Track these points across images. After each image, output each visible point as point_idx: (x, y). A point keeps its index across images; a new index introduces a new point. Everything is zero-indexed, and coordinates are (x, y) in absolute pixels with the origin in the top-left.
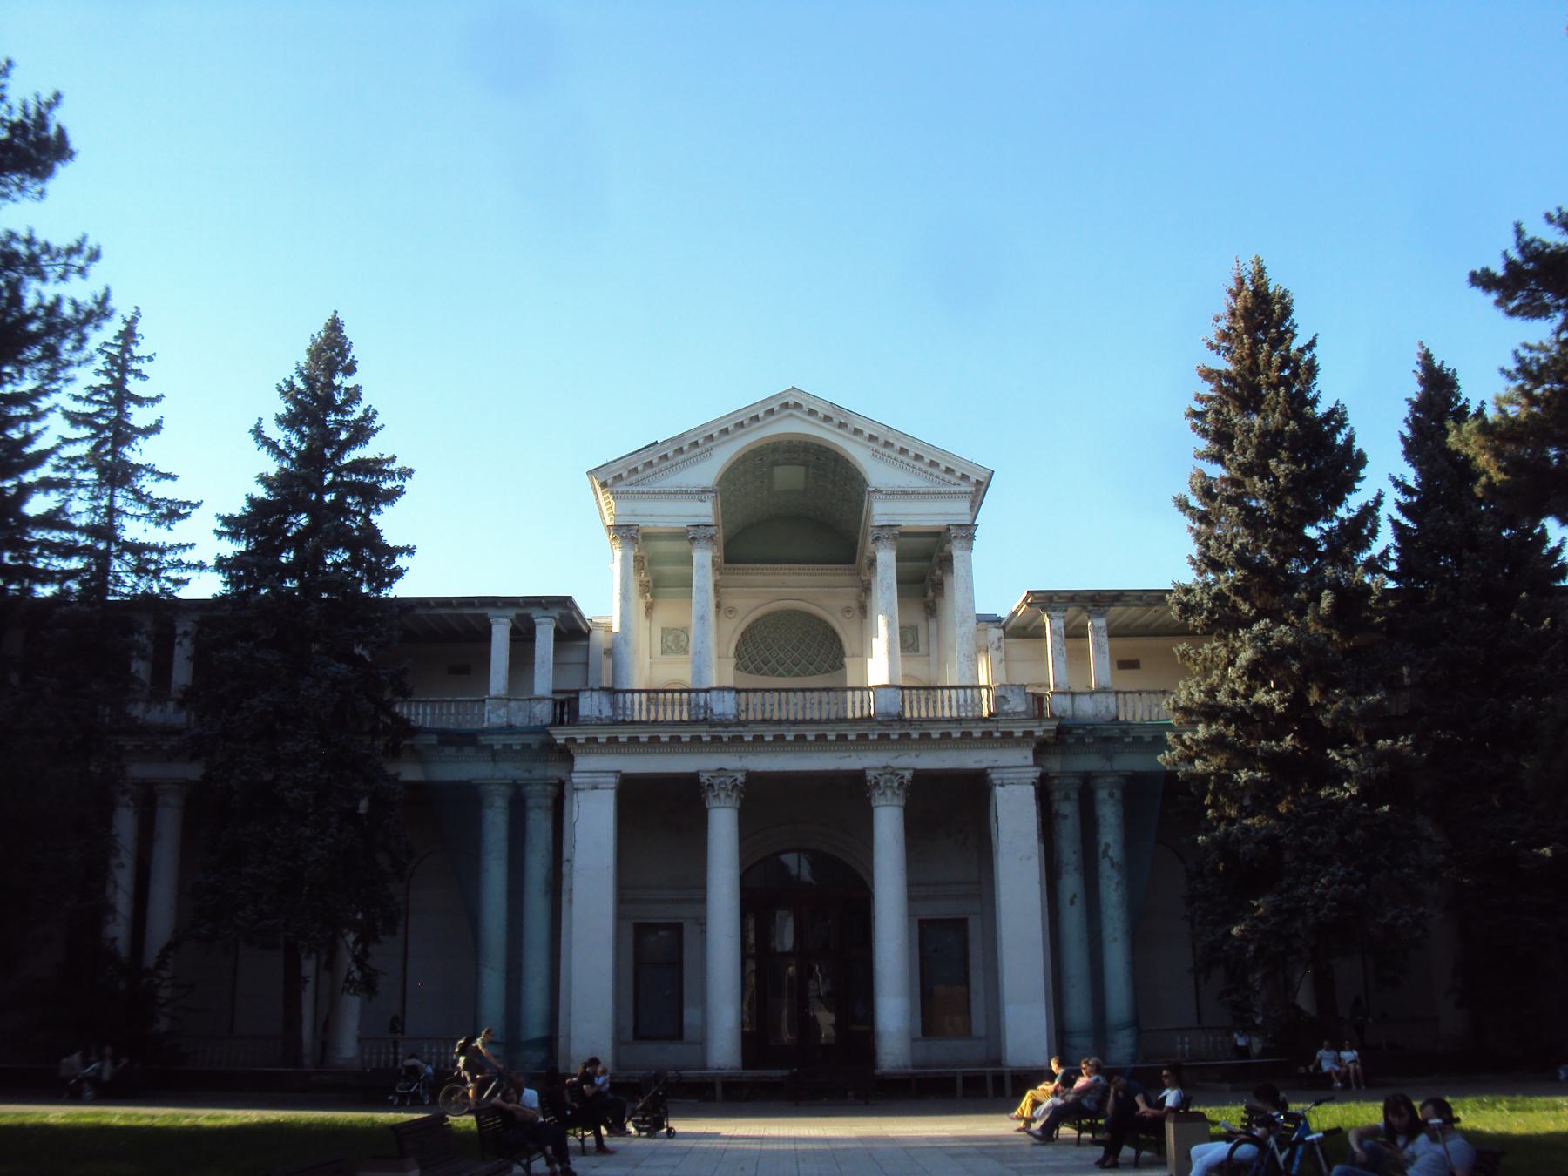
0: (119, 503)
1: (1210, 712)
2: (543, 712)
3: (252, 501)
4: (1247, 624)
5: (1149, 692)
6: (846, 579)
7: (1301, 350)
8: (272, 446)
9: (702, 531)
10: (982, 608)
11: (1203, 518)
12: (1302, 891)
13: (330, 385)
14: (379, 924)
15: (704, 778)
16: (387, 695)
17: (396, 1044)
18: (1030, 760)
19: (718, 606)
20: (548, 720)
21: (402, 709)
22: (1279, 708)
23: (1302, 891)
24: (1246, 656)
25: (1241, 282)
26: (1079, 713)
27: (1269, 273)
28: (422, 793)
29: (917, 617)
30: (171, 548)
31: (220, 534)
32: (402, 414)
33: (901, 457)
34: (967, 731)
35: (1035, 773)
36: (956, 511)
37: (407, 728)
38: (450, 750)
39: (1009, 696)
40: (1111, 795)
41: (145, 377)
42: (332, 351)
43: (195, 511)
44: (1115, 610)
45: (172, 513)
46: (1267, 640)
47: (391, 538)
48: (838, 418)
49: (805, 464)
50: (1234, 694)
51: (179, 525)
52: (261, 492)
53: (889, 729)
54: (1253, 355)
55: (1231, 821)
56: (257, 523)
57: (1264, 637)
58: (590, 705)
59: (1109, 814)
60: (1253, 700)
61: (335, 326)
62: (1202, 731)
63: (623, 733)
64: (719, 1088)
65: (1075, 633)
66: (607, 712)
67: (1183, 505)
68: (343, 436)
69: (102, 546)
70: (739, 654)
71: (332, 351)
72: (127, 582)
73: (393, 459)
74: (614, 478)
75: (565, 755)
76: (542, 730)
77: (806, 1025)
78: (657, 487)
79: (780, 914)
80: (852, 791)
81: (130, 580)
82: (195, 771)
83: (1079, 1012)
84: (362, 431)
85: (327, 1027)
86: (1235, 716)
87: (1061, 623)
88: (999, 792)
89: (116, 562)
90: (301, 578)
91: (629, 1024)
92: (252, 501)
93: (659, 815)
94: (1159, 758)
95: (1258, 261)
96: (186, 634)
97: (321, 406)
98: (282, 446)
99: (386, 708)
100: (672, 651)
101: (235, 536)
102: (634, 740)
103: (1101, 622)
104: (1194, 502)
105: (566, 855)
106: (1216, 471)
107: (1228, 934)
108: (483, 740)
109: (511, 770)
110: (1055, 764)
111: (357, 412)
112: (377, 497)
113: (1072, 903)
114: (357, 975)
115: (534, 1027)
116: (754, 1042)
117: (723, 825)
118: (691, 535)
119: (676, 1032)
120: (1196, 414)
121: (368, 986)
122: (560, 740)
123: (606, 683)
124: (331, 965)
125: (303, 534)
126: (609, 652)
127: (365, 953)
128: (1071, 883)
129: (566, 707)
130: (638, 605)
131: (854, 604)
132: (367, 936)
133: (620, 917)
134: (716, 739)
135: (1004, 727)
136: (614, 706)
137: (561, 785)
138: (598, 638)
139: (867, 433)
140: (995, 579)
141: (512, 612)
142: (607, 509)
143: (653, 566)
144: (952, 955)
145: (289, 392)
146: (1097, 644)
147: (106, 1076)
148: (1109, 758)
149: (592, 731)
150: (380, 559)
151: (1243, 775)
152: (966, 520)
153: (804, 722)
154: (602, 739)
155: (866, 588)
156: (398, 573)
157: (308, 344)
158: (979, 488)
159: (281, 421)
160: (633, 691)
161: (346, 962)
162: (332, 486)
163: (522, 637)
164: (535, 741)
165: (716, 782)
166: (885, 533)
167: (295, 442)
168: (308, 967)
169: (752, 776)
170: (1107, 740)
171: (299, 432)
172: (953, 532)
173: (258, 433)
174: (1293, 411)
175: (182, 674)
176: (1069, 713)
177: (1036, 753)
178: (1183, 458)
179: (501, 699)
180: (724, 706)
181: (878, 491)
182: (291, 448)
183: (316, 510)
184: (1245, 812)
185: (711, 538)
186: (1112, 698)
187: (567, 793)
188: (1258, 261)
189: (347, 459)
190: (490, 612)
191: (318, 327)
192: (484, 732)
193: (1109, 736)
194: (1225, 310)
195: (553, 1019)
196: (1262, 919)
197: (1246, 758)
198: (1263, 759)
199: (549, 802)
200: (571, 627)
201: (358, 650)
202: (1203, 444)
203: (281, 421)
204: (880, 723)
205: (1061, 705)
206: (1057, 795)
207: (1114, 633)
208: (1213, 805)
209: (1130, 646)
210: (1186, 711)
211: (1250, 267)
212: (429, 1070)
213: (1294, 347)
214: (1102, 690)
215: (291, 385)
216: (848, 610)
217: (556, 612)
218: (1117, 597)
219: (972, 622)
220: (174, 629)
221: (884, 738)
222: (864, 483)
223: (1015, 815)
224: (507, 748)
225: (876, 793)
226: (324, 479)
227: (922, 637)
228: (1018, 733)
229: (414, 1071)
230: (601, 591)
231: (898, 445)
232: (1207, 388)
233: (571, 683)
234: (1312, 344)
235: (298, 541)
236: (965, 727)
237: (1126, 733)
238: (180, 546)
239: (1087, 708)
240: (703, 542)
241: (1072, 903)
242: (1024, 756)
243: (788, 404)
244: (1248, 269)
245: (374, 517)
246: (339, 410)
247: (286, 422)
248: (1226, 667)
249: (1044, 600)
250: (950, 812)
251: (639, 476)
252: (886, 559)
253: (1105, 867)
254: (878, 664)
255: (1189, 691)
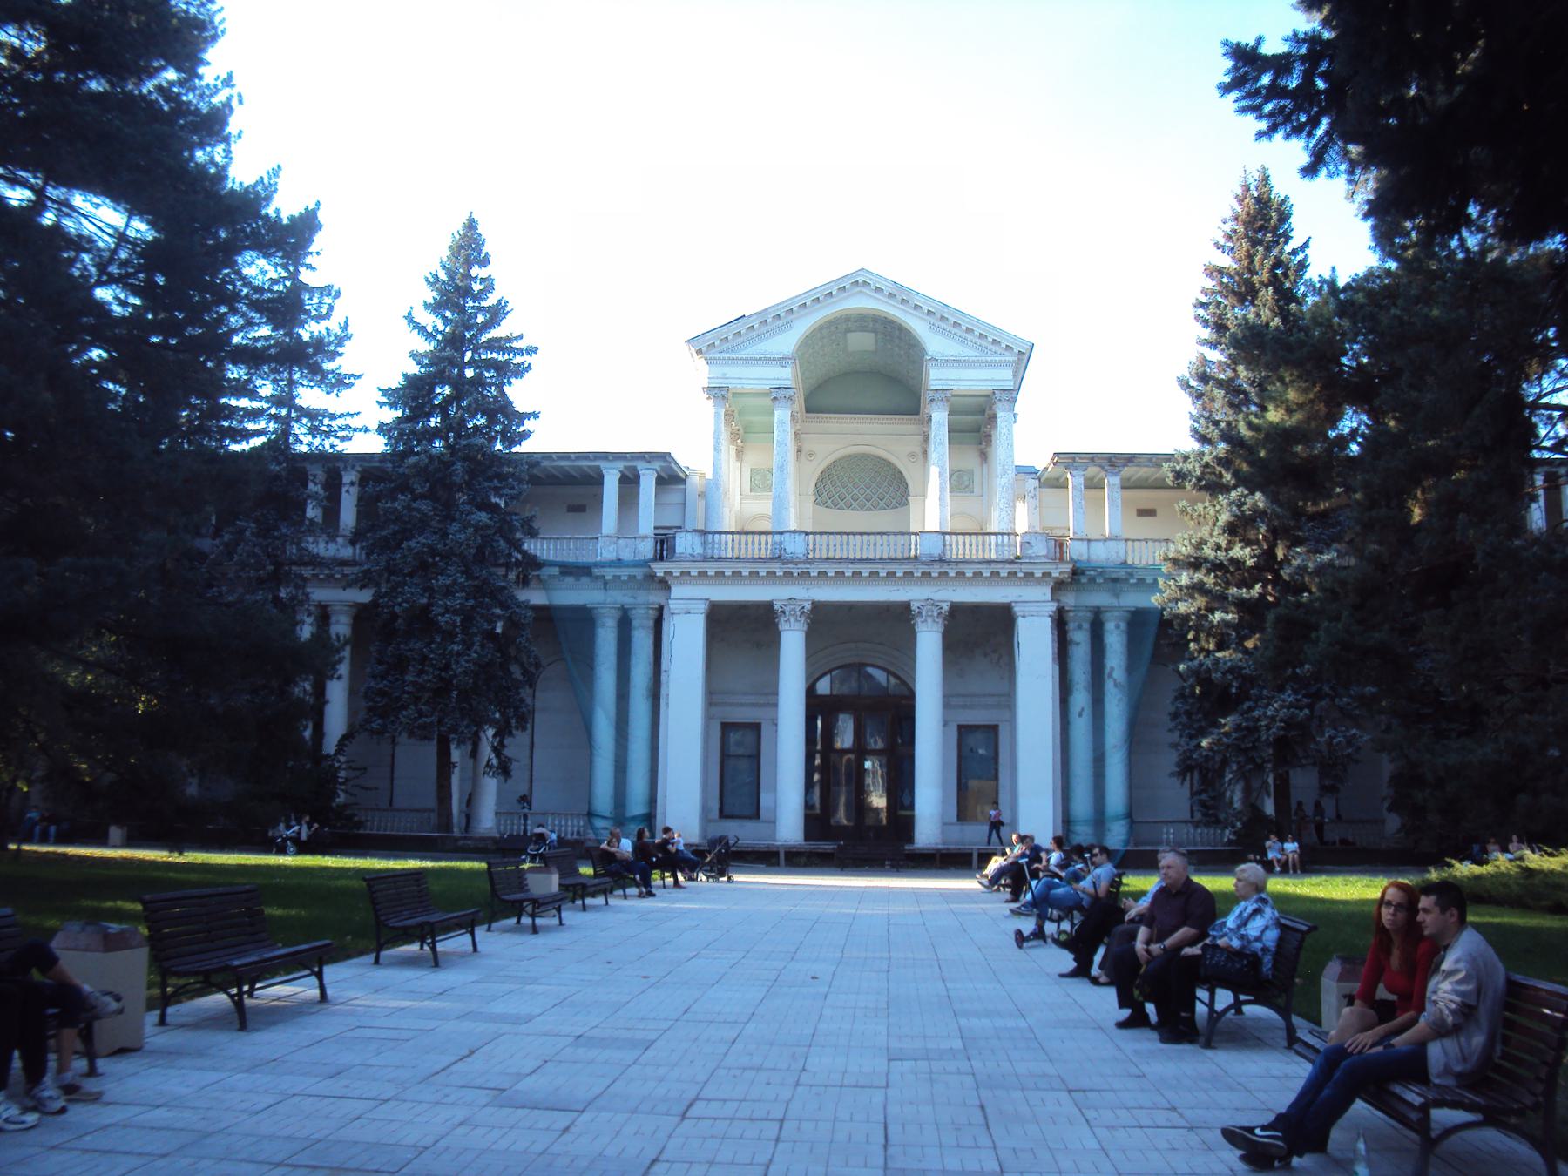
0: (296, 377)
1: (1195, 564)
2: (647, 549)
3: (406, 376)
4: (1226, 489)
5: (1146, 541)
6: (912, 428)
7: (1294, 252)
8: (422, 329)
9: (783, 392)
10: (1022, 460)
11: (1200, 396)
12: (1256, 713)
13: (467, 276)
14: (513, 722)
15: (777, 607)
16: (518, 535)
17: (525, 817)
18: (1048, 597)
19: (799, 451)
20: (650, 555)
21: (530, 546)
22: (1250, 563)
23: (1256, 713)
24: (1224, 518)
25: (1247, 188)
26: (1093, 557)
27: (1273, 181)
28: (546, 615)
29: (970, 460)
30: (341, 415)
31: (381, 404)
32: (530, 300)
33: (954, 330)
34: (993, 571)
35: (1052, 607)
36: (1004, 377)
37: (533, 563)
38: (570, 580)
39: (1033, 542)
40: (1117, 627)
41: (314, 269)
42: (469, 247)
43: (357, 382)
44: (1128, 471)
45: (341, 382)
46: (1240, 504)
47: (520, 406)
48: (899, 294)
49: (875, 331)
50: (1218, 547)
51: (346, 393)
52: (414, 369)
53: (940, 567)
54: (1250, 257)
55: (1208, 652)
56: (414, 396)
57: (1240, 504)
58: (685, 544)
59: (1115, 641)
60: (1231, 553)
61: (471, 225)
62: (1184, 578)
63: (712, 566)
64: (782, 856)
65: (1093, 485)
66: (699, 550)
67: (1185, 385)
68: (480, 319)
69: (284, 412)
70: (818, 491)
71: (469, 247)
72: (304, 442)
73: (521, 337)
74: (710, 345)
75: (664, 584)
76: (645, 564)
77: (860, 806)
78: (745, 354)
79: (841, 716)
80: (899, 618)
81: (307, 439)
82: (365, 596)
83: (1082, 805)
84: (497, 314)
85: (470, 801)
86: (1216, 567)
87: (1082, 480)
88: (1021, 622)
89: (296, 426)
90: (446, 439)
91: (715, 805)
92: (406, 376)
93: (740, 631)
94: (1153, 599)
95: (1264, 170)
96: (352, 484)
97: (461, 295)
98: (430, 329)
99: (517, 545)
100: (755, 492)
101: (393, 405)
102: (720, 574)
103: (1116, 480)
104: (1193, 383)
105: (664, 667)
106: (1215, 356)
107: (1199, 746)
108: (596, 571)
109: (619, 597)
110: (1069, 600)
111: (491, 300)
112: (507, 371)
113: (1080, 715)
114: (495, 762)
115: (637, 807)
116: (816, 822)
117: (793, 643)
118: (777, 395)
119: (754, 813)
120: (1203, 305)
121: (504, 770)
122: (660, 574)
123: (701, 526)
124: (474, 754)
125: (448, 401)
126: (702, 495)
127: (501, 744)
128: (1081, 699)
129: (664, 544)
130: (729, 451)
131: (918, 450)
132: (503, 732)
133: (708, 718)
134: (788, 574)
135: (1026, 568)
136: (705, 544)
137: (661, 609)
138: (694, 480)
139: (926, 308)
140: (1029, 438)
141: (621, 465)
142: (700, 373)
143: (740, 418)
144: (980, 757)
145: (434, 282)
146: (1111, 499)
147: (304, 837)
148: (1117, 596)
149: (686, 566)
150: (506, 418)
151: (1218, 616)
152: (1010, 385)
153: (861, 560)
154: (694, 573)
155: (926, 438)
156: (526, 435)
157: (449, 242)
158: (1022, 358)
159: (427, 306)
160: (720, 533)
161: (486, 752)
162: (471, 363)
163: (629, 482)
164: (639, 573)
165: (787, 609)
166: (937, 396)
167: (441, 328)
168: (456, 755)
169: (818, 607)
170: (1115, 580)
171: (444, 317)
172: (998, 394)
173: (410, 318)
174: (1280, 308)
175: (348, 516)
176: (1085, 557)
177: (1053, 590)
178: (1185, 343)
179: (614, 537)
180: (795, 547)
181: (933, 359)
182: (438, 332)
183: (460, 385)
184: (1221, 646)
185: (790, 398)
186: (1122, 545)
187: (665, 616)
188: (1264, 170)
189: (484, 338)
190: (602, 464)
191: (457, 226)
192: (596, 565)
193: (1118, 578)
194: (1229, 214)
195: (652, 800)
196: (1226, 734)
197: (1218, 600)
198: (1235, 604)
199: (651, 623)
200: (671, 478)
201: (494, 500)
202: (1206, 333)
203: (427, 306)
204: (923, 563)
205: (1076, 550)
206: (1071, 626)
207: (1127, 485)
208: (1196, 639)
209: (1146, 497)
210: (1175, 561)
211: (1256, 175)
212: (554, 836)
213: (1288, 248)
214: (1115, 538)
215: (436, 277)
216: (913, 455)
217: (657, 465)
218: (1130, 459)
219: (1011, 474)
220: (340, 477)
221: (926, 575)
222: (923, 351)
223: (1034, 642)
224: (617, 578)
225: (919, 620)
226: (463, 372)
227: (977, 479)
228: (1038, 574)
229: (541, 837)
230: (695, 443)
231: (952, 320)
232: (1210, 284)
233: (671, 519)
234: (1305, 245)
235: (443, 409)
236: (995, 568)
237: (1131, 575)
238: (349, 414)
239: (1102, 554)
240: (783, 402)
241: (1080, 715)
242: (1043, 593)
243: (858, 282)
244: (1254, 178)
245: (506, 388)
246: (476, 297)
247: (436, 308)
248: (1203, 525)
249: (1069, 460)
250: (981, 635)
251: (729, 345)
252: (940, 418)
253: (1109, 686)
254: (932, 509)
255: (1182, 547)
